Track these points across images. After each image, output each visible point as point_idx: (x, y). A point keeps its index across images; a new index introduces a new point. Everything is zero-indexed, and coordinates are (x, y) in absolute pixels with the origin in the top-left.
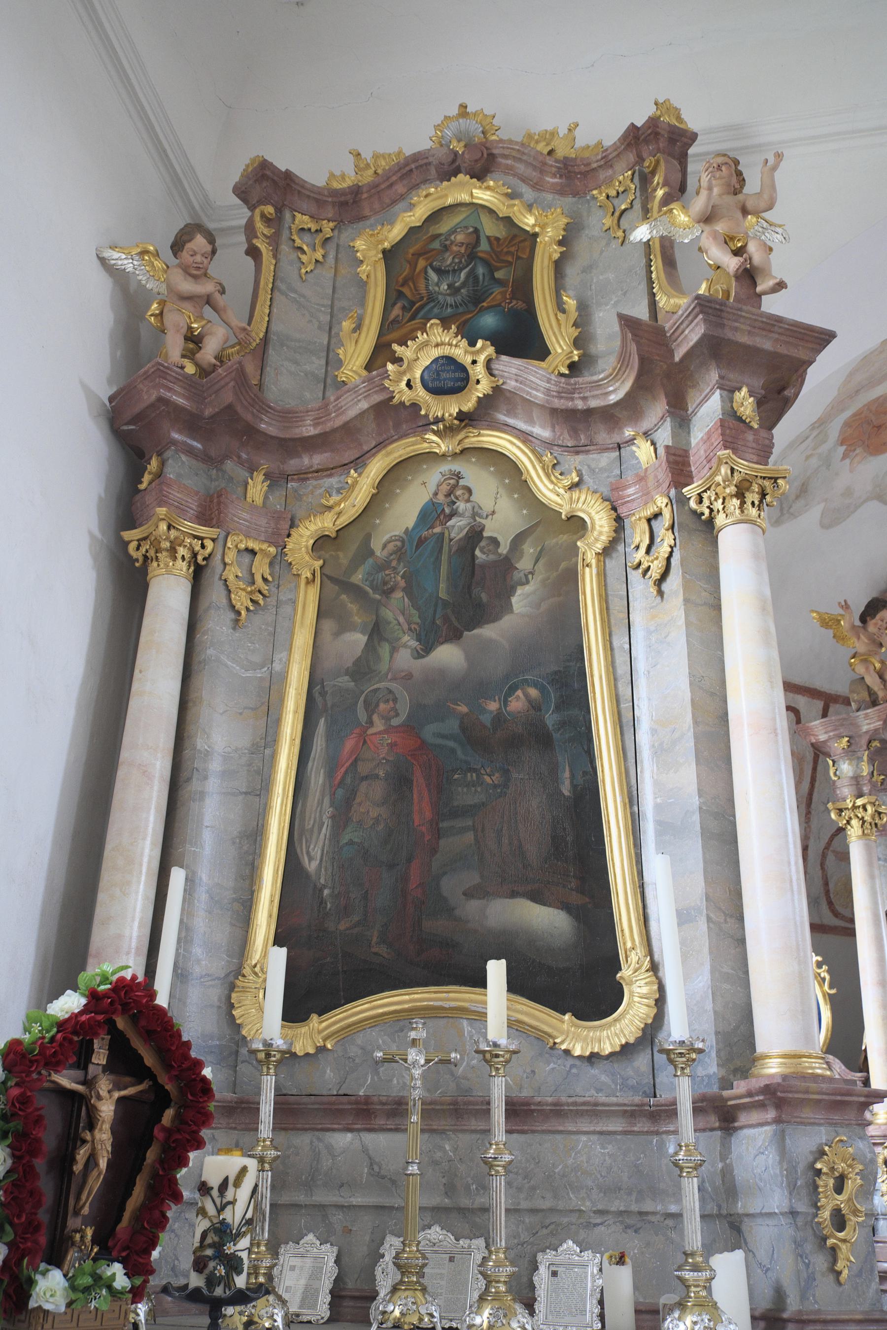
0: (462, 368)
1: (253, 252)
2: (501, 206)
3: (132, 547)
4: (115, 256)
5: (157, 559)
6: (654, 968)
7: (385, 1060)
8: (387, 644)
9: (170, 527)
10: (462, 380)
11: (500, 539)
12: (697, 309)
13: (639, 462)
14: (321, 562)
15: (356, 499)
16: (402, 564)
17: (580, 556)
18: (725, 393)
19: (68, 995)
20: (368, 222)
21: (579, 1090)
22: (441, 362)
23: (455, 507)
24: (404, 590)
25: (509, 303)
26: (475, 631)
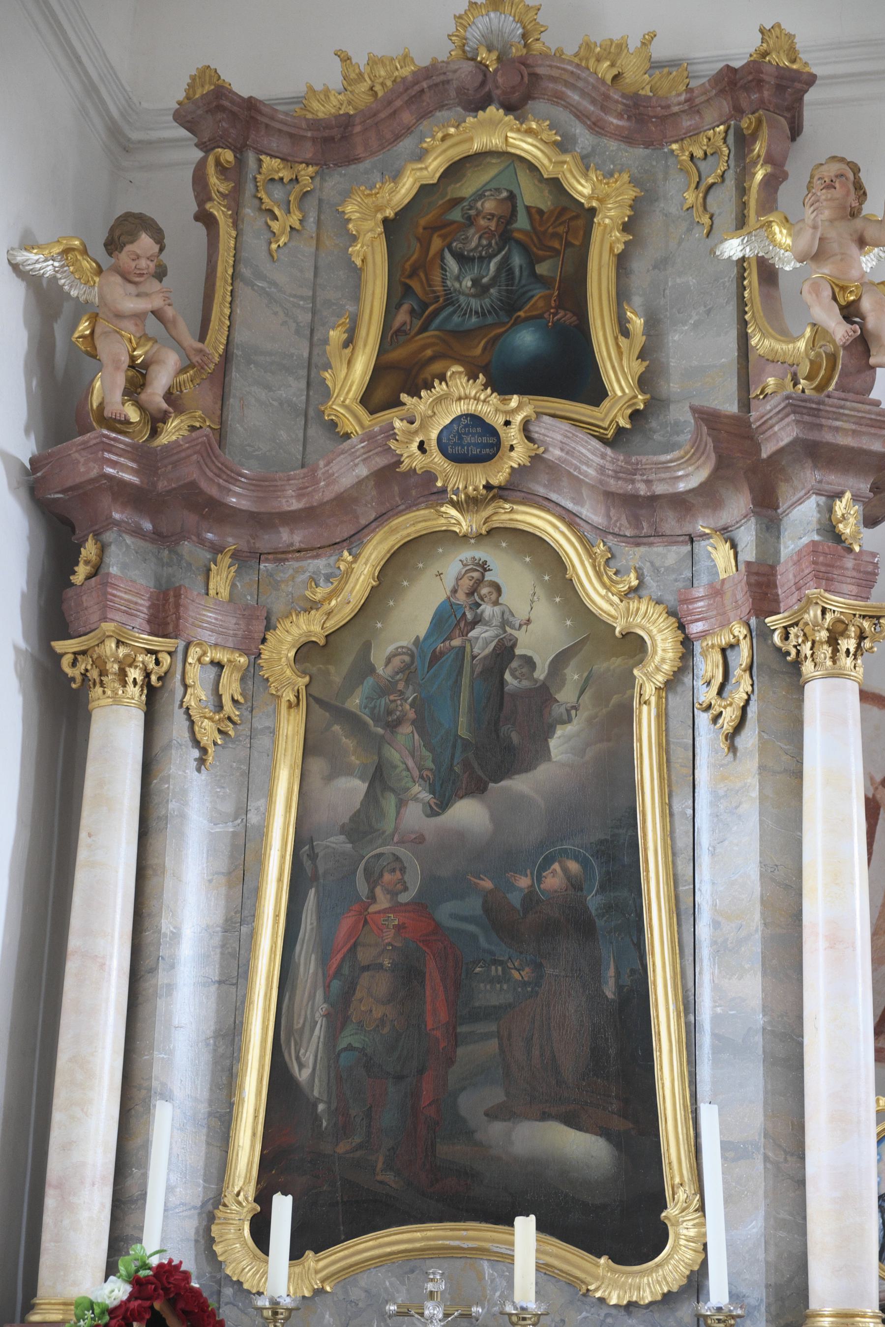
0: (492, 431)
1: (206, 219)
2: (546, 162)
3: (66, 662)
4: (31, 258)
5: (102, 684)
7: (399, 1314)
8: (393, 796)
9: (119, 643)
10: (491, 446)
11: (536, 659)
12: (788, 409)
13: (715, 566)
14: (307, 679)
15: (351, 592)
16: (411, 687)
17: (637, 689)
18: (822, 500)
19: (112, 1282)
20: (361, 167)
22: (464, 421)
23: (479, 611)
24: (413, 723)
25: (555, 314)
26: (503, 783)
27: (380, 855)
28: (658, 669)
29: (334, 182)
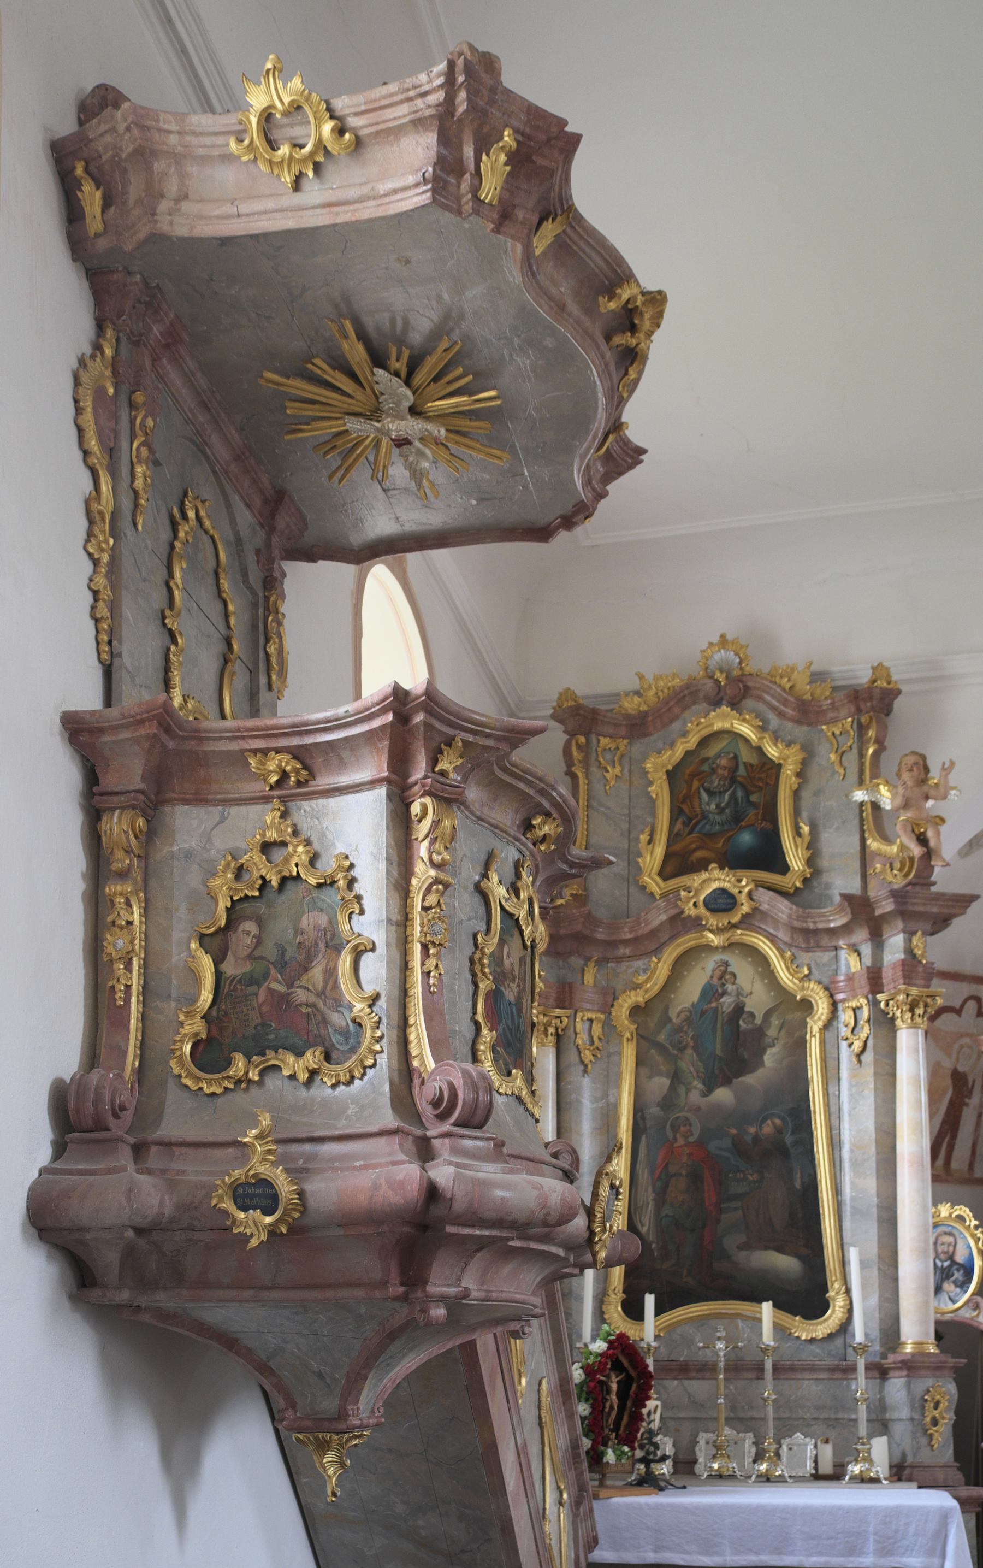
0: (732, 896)
2: (754, 737)
6: (848, 1291)
7: (703, 1347)
18: (907, 935)
20: (652, 738)
21: (804, 1357)
26: (741, 1079)
27: (677, 1118)
28: (819, 1018)
29: (637, 748)
